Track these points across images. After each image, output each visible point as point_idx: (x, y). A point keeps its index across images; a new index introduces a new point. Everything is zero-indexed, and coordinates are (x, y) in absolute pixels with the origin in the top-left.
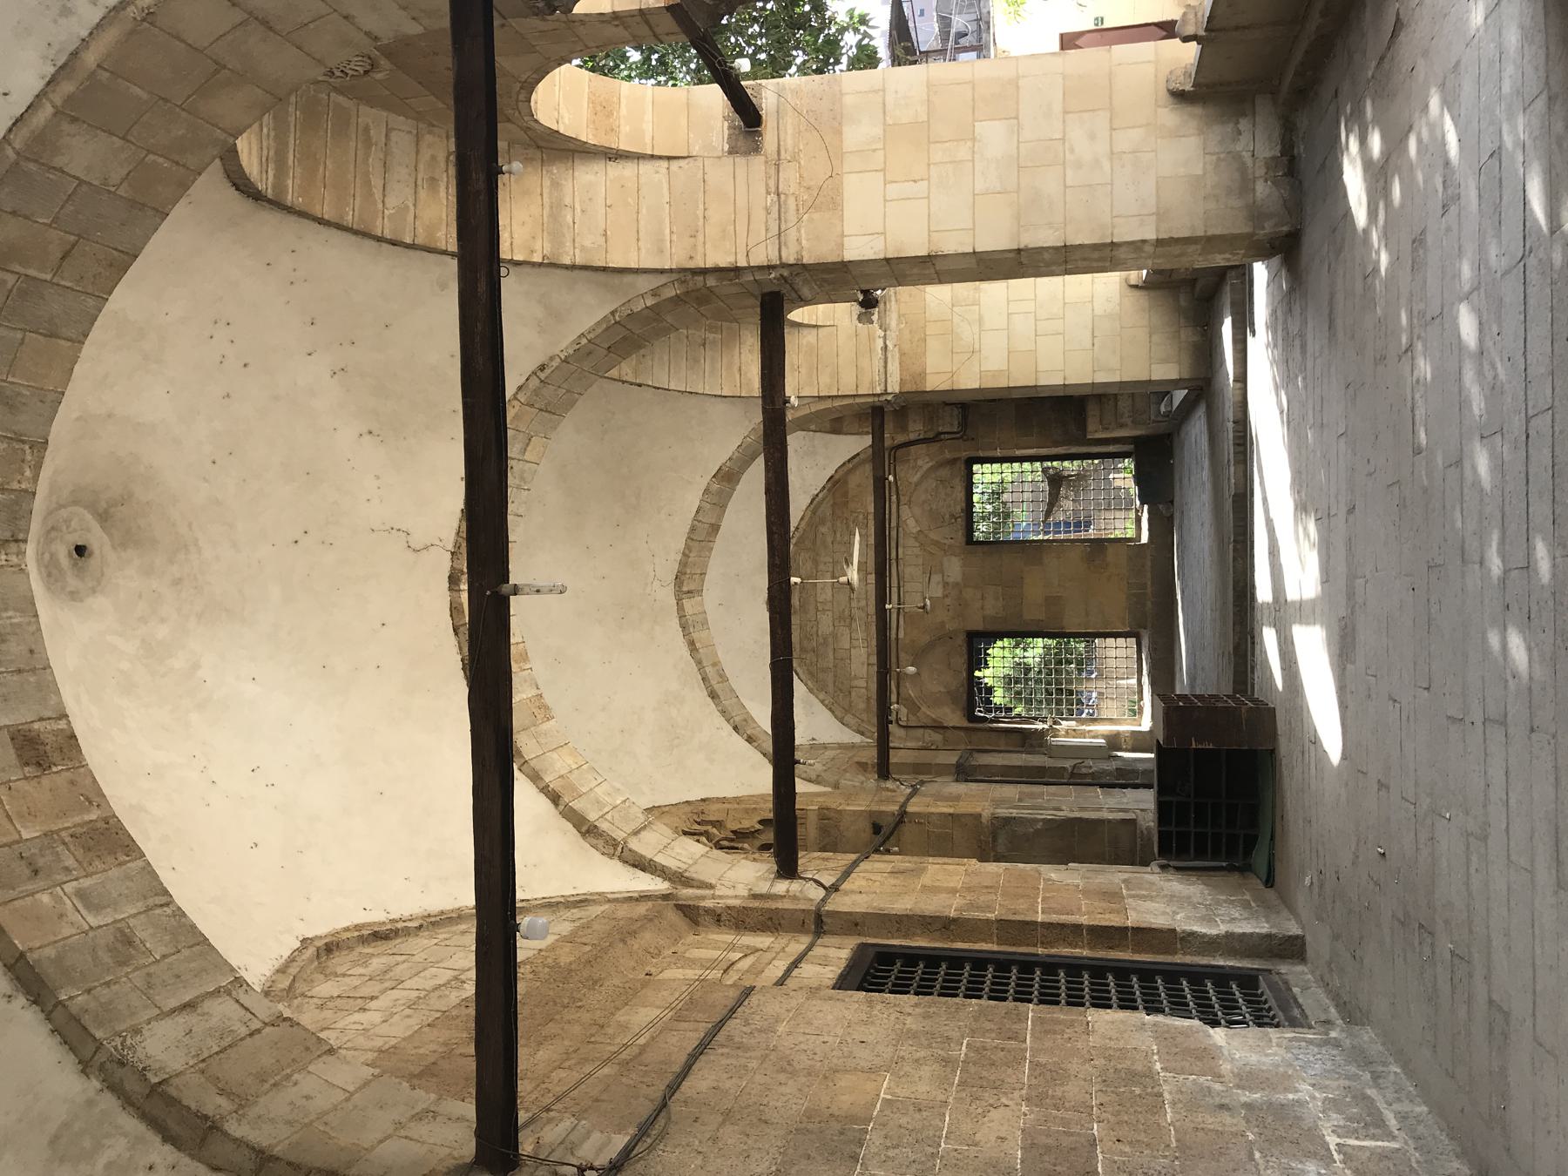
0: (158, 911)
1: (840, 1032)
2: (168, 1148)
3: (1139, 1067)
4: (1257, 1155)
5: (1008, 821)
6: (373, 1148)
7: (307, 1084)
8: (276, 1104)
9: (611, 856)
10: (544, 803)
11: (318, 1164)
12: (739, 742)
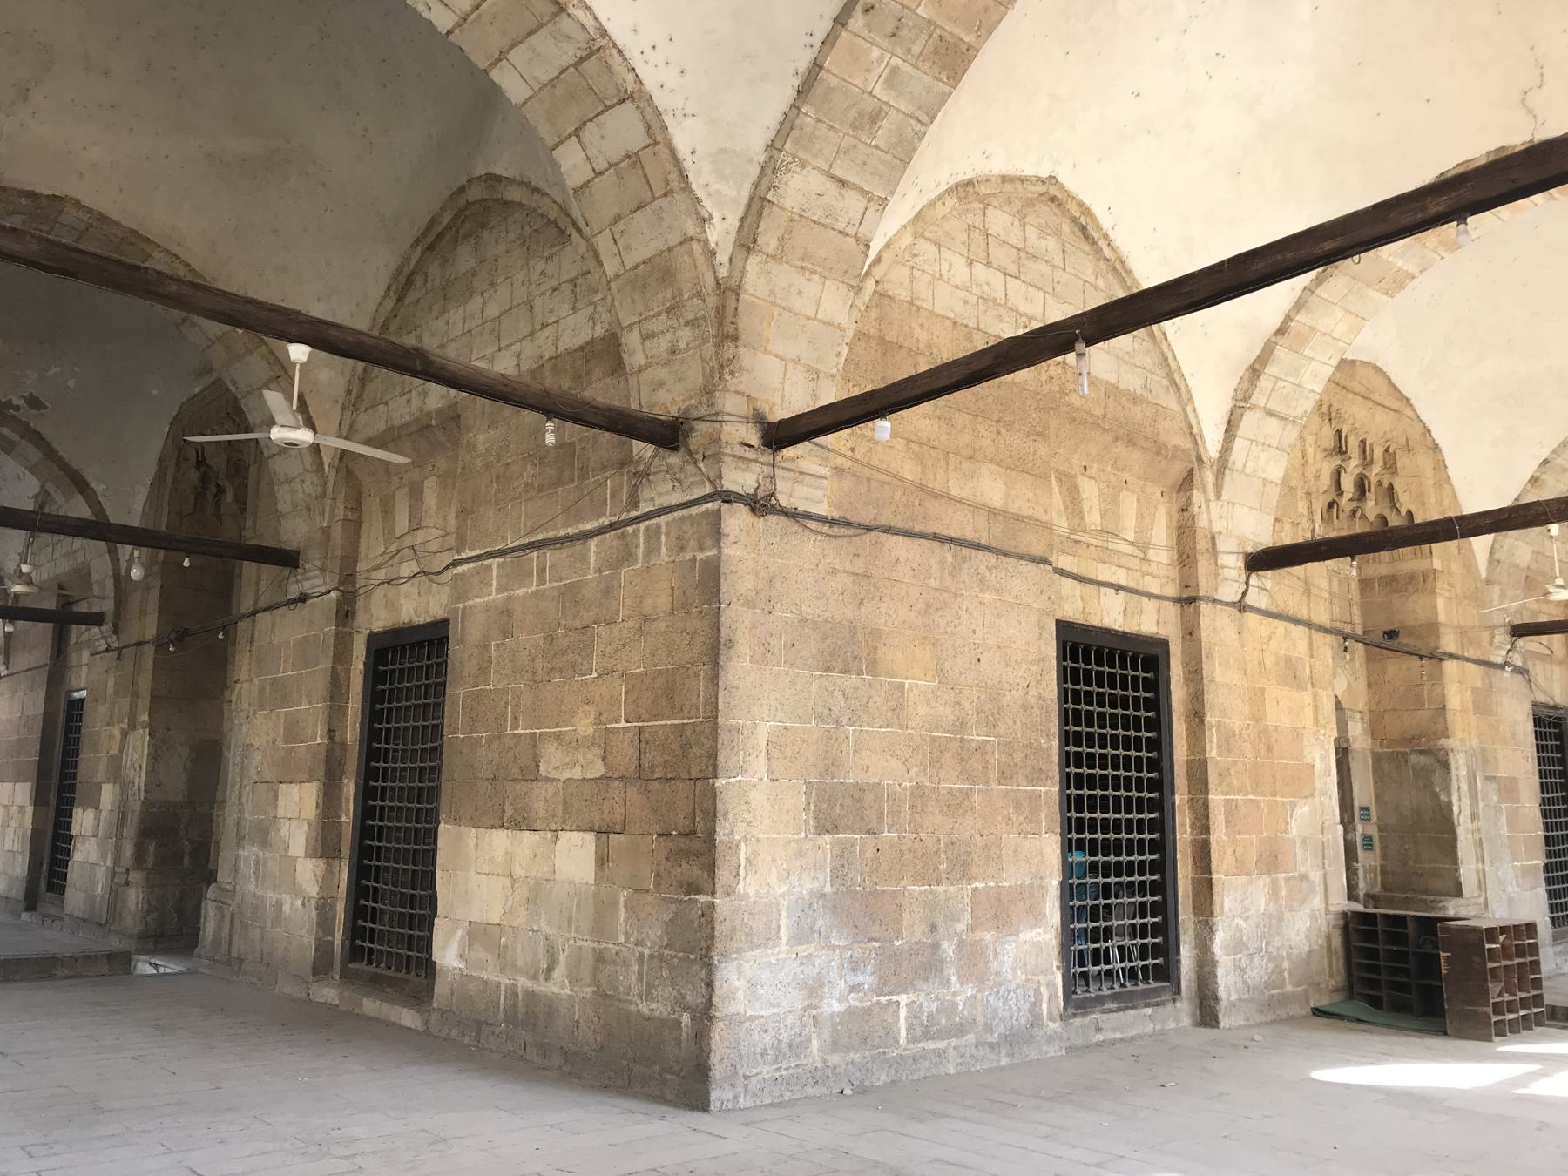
0: (913, 122)
1: (992, 641)
2: (737, 224)
3: (974, 870)
4: (876, 944)
5: (1446, 766)
6: (770, 353)
7: (813, 287)
8: (784, 276)
9: (1235, 398)
10: (1276, 321)
11: (740, 325)
12: (1530, 468)
